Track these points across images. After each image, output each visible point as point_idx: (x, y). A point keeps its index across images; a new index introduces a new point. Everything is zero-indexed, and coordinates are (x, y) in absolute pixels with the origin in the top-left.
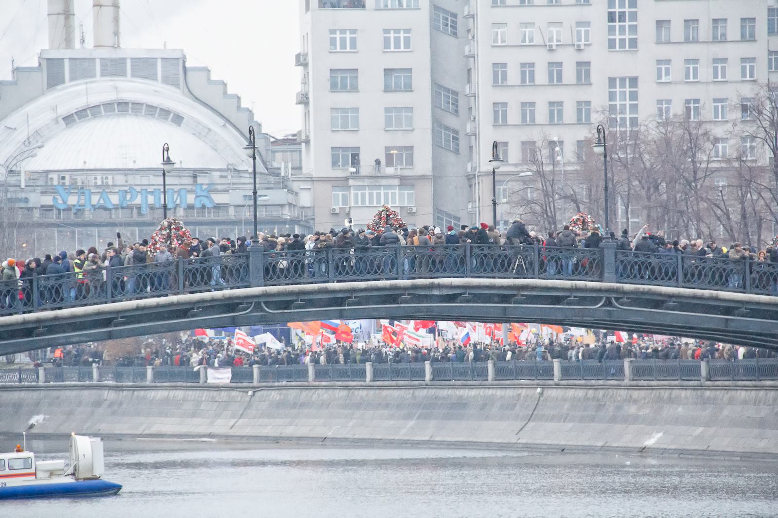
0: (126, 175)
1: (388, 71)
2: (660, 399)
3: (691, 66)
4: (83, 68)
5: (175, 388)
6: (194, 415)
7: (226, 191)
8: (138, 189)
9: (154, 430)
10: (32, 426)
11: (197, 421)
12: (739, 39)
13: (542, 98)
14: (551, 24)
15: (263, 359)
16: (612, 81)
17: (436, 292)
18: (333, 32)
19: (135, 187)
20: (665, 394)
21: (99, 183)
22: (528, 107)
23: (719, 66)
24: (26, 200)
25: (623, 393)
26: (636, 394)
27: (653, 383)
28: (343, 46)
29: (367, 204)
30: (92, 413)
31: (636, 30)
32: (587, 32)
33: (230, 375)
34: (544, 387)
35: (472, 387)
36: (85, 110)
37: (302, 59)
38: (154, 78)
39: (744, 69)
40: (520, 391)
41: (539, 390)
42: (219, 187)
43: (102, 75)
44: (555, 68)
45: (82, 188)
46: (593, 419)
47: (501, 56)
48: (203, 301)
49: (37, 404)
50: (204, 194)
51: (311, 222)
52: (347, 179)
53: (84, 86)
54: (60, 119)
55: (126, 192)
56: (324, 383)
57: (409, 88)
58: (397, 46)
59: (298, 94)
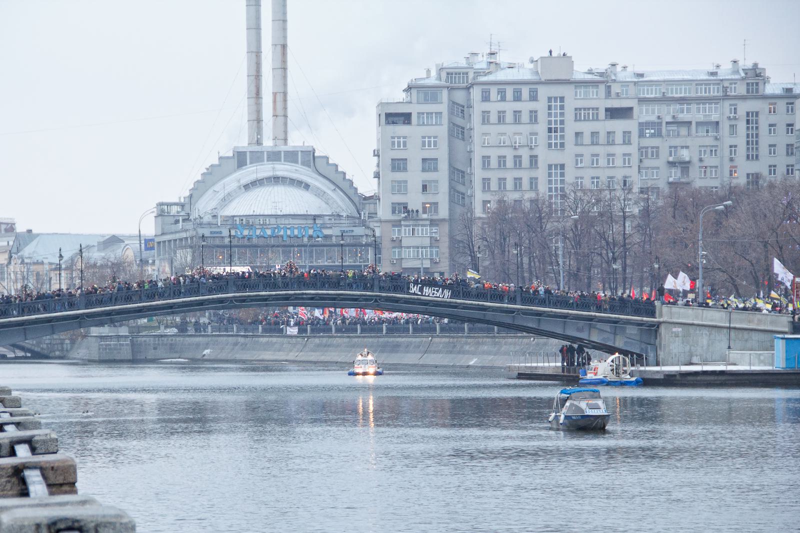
0: (276, 218)
1: (424, 160)
2: (478, 343)
3: (595, 158)
4: (257, 157)
5: (271, 336)
6: (279, 350)
7: (331, 228)
8: (282, 226)
9: (261, 358)
10: (204, 355)
11: (281, 353)
12: (622, 143)
13: (510, 176)
14: (515, 134)
15: (315, 322)
16: (550, 166)
17: (305, 296)
18: (393, 138)
19: (280, 226)
20: (480, 340)
21: (262, 223)
22: (502, 181)
23: (611, 158)
24: (221, 233)
25: (464, 339)
26: (469, 340)
27: (476, 335)
28: (399, 145)
29: (407, 235)
30: (233, 349)
31: (564, 138)
32: (536, 139)
33: (297, 330)
34: (432, 337)
35: (402, 337)
36: (256, 181)
37: (376, 153)
38: (296, 162)
39: (624, 160)
40: (423, 339)
41: (430, 338)
42: (328, 226)
43: (268, 161)
44: (518, 159)
45: (252, 225)
46: (451, 352)
47: (486, 152)
48: (209, 299)
49: (207, 344)
50: (319, 229)
51: (380, 245)
52: (400, 221)
53: (255, 168)
54: (242, 187)
55: (275, 228)
56: (339, 335)
57: (436, 169)
58: (429, 145)
59: (374, 172)
